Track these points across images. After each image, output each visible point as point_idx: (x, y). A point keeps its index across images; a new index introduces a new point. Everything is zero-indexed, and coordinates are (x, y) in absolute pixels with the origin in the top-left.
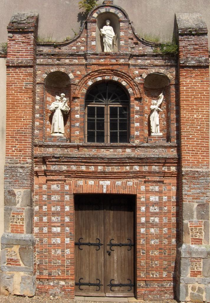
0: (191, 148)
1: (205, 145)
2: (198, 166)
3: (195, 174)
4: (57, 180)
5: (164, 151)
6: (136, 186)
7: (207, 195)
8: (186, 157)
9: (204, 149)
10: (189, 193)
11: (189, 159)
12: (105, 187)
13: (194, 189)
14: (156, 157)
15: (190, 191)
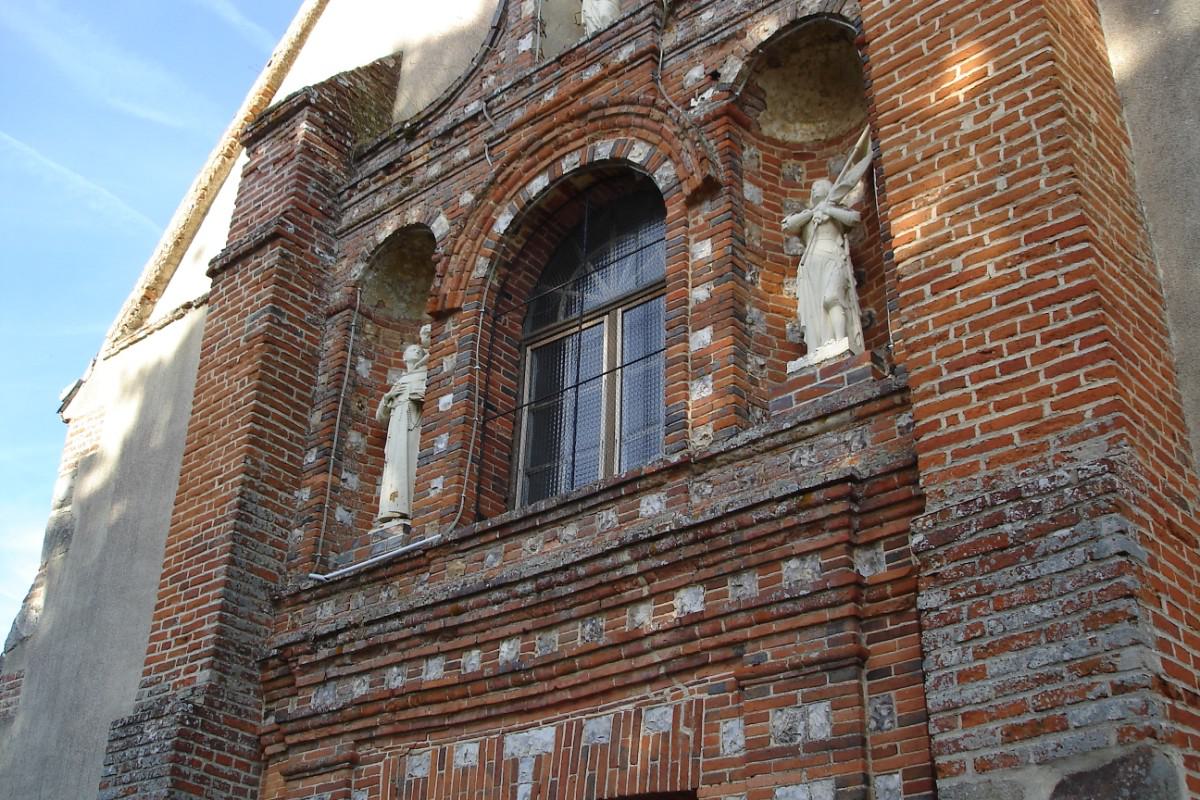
0: (972, 343)
1: (1063, 285)
2: (1036, 457)
3: (1000, 519)
4: (318, 768)
5: (855, 444)
6: (689, 732)
7: (1117, 678)
8: (942, 417)
9: (1060, 316)
10: (971, 691)
11: (964, 424)
12: (526, 769)
13: (1004, 646)
14: (784, 492)
15: (979, 674)
